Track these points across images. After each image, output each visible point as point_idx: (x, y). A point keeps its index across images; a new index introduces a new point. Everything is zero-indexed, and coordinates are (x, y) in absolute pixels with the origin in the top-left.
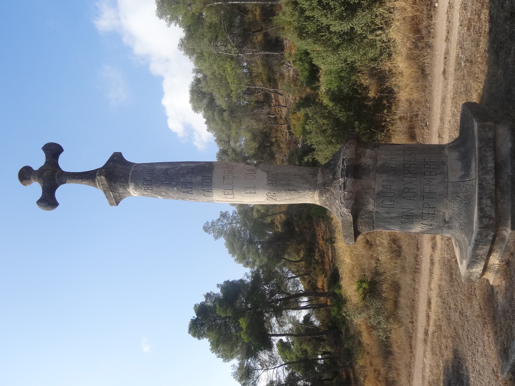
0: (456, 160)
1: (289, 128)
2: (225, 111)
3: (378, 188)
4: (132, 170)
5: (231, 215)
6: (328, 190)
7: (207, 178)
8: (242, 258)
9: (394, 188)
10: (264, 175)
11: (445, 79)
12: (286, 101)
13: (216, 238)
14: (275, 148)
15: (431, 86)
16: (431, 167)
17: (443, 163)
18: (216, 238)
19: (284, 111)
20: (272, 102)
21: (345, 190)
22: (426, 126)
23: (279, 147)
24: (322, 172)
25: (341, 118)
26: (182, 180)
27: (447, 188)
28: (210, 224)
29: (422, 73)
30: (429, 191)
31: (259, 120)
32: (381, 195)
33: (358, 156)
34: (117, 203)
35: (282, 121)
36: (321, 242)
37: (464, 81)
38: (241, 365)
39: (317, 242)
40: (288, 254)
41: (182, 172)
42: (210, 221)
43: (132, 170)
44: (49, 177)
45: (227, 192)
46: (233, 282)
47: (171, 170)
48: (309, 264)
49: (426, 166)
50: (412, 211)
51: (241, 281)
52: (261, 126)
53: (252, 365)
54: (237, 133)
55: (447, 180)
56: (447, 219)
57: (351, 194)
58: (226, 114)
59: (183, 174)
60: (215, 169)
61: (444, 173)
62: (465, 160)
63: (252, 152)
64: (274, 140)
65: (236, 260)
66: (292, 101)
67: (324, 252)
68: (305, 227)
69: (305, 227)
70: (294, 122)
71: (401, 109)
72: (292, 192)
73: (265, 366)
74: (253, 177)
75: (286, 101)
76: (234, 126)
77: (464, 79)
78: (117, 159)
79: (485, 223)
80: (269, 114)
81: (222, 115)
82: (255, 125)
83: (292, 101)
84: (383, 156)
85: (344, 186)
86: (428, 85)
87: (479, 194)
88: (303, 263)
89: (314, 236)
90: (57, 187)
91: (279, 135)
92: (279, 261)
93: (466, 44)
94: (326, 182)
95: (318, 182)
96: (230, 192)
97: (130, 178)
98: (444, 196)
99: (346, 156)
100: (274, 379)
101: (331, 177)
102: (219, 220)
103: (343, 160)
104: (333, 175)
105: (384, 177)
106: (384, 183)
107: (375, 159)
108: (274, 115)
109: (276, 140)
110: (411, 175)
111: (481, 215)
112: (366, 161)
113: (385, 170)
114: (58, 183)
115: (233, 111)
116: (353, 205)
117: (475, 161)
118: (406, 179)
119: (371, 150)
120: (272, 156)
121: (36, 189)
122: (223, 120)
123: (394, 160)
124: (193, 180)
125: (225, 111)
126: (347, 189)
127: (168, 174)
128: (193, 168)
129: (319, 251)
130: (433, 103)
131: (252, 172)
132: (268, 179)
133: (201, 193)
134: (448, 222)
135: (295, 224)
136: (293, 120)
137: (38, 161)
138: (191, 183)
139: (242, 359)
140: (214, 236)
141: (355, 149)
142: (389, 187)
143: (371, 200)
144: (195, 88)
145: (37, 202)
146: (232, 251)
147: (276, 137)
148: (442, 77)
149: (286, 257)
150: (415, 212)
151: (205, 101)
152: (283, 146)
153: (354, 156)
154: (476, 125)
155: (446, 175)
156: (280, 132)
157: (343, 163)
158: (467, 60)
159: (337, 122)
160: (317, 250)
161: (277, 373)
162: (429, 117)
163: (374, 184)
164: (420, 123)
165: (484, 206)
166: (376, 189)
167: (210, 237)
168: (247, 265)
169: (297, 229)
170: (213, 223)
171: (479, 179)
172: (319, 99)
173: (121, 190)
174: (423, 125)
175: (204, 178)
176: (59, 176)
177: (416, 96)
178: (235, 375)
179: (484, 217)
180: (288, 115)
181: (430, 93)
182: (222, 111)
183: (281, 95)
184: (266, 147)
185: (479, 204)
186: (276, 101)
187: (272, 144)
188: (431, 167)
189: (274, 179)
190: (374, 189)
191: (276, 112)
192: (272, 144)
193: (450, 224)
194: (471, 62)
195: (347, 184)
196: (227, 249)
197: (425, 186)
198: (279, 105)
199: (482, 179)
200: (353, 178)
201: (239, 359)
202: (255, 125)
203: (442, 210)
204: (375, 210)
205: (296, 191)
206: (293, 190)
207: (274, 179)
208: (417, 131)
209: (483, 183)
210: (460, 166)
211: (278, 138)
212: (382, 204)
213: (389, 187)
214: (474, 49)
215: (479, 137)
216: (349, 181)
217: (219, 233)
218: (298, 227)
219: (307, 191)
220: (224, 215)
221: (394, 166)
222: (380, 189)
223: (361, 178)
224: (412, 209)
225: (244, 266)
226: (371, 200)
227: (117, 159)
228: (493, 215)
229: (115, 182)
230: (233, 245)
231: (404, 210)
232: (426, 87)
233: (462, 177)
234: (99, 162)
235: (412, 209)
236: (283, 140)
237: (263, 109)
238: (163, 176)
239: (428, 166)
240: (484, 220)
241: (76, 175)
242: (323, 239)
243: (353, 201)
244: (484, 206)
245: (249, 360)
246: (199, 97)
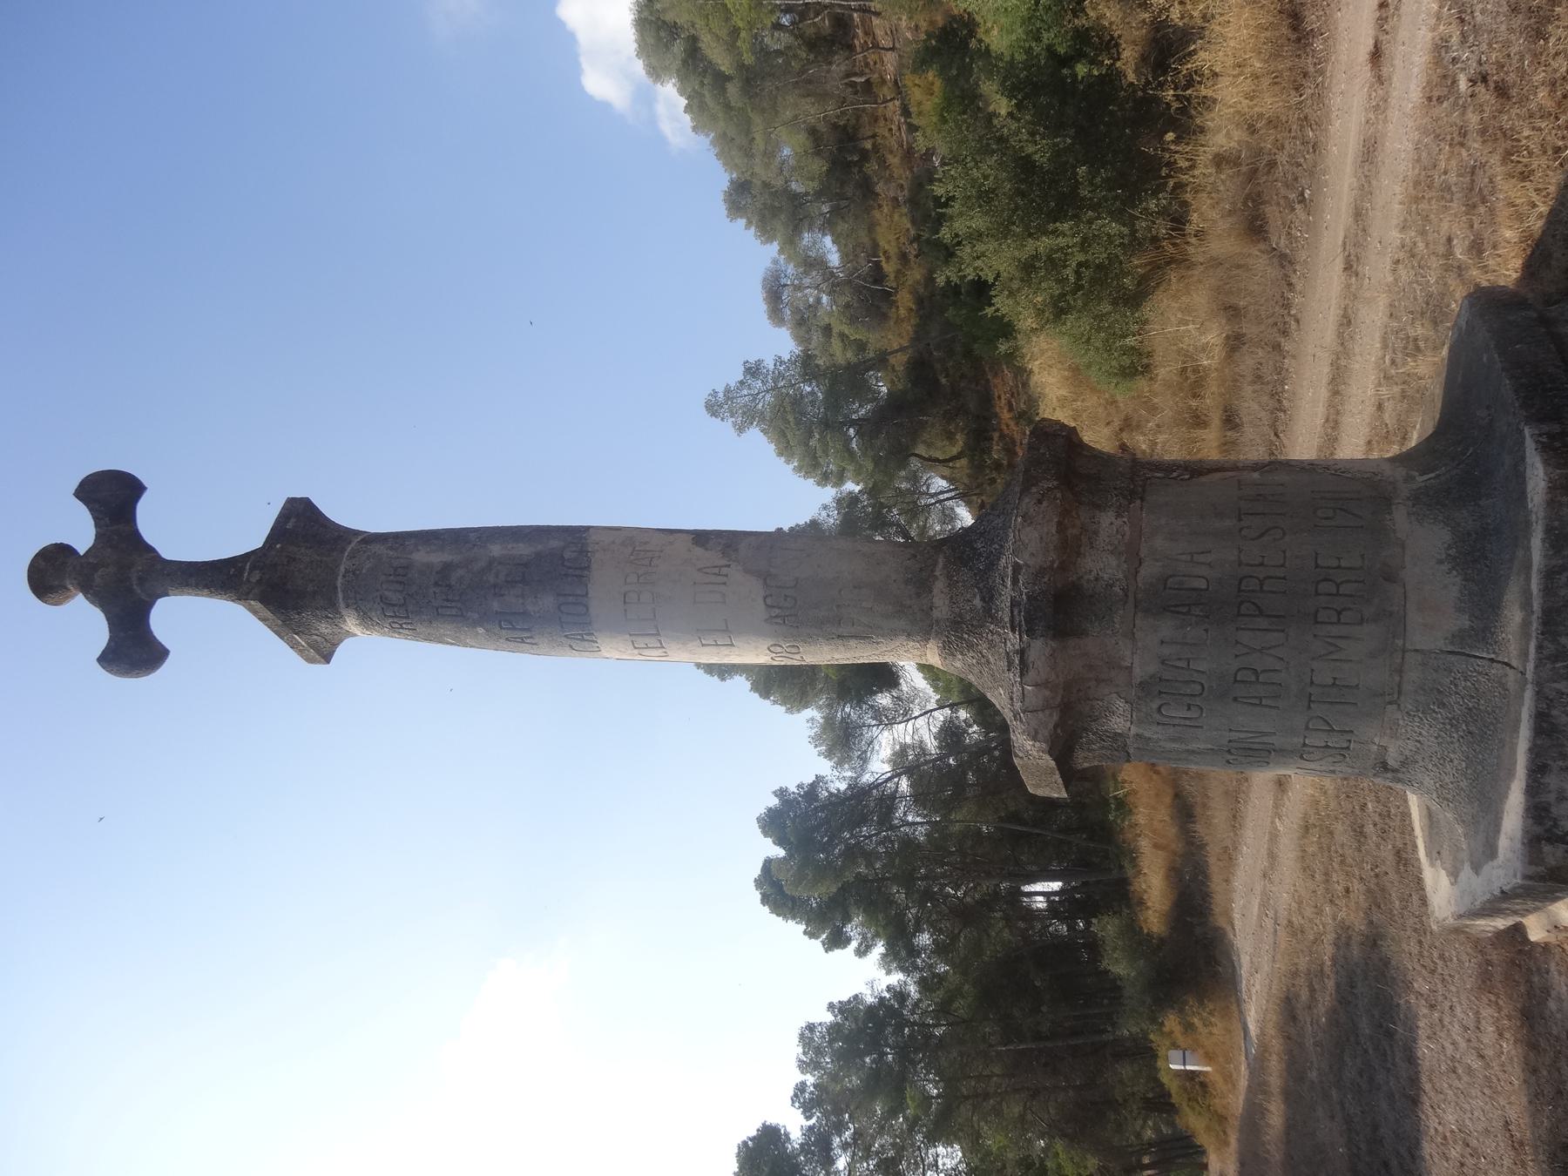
0: (1440, 562)
1: (906, 112)
2: (729, 78)
3: (1143, 667)
4: (342, 569)
5: (771, 367)
6: (971, 646)
7: (571, 599)
8: (812, 466)
9: (1203, 666)
11: (1380, 80)
12: (894, 32)
13: (741, 429)
14: (872, 167)
15: (1322, 72)
17: (1390, 577)
18: (741, 429)
19: (890, 61)
20: (855, 36)
21: (1028, 678)
22: (1302, 200)
23: (883, 162)
24: (949, 577)
25: (1036, 157)
26: (496, 605)
27: (1400, 672)
28: (721, 395)
29: (1295, 28)
30: (1330, 681)
31: (823, 97)
32: (1148, 688)
33: (1069, 547)
34: (327, 658)
35: (885, 90)
36: (1006, 415)
37: (1464, 153)
38: (829, 722)
39: (996, 415)
40: (924, 442)
41: (492, 579)
42: (721, 389)
43: (342, 569)
44: (114, 572)
45: (641, 642)
46: (791, 529)
47: (460, 572)
48: (978, 468)
49: (1323, 587)
50: (1265, 739)
51: (814, 524)
52: (831, 110)
53: (854, 716)
54: (768, 140)
55: (1400, 642)
56: (1391, 763)
57: (1047, 693)
58: (733, 90)
59: (495, 586)
60: (594, 566)
61: (1391, 614)
62: (1480, 562)
63: (813, 185)
64: (868, 145)
65: (798, 469)
66: (909, 35)
67: (1013, 442)
68: (963, 376)
69: (963, 376)
70: (916, 94)
71: (1222, 132)
72: (853, 643)
73: (886, 719)
75: (894, 32)
76: (757, 119)
77: (1462, 145)
78: (301, 524)
79: (1551, 861)
80: (848, 75)
81: (724, 90)
82: (812, 112)
83: (909, 35)
85: (1022, 661)
86: (1311, 69)
87: (1535, 752)
88: (964, 462)
89: (987, 400)
91: (881, 130)
92: (903, 464)
93: (1483, 12)
94: (960, 615)
95: (936, 614)
96: (653, 642)
97: (340, 595)
98: (1388, 698)
99: (1026, 556)
100: (908, 740)
101: (977, 602)
102: (742, 383)
103: (1017, 569)
104: (983, 599)
105: (1167, 627)
107: (1132, 555)
108: (862, 74)
109: (874, 145)
110: (1263, 623)
111: (1539, 830)
112: (1101, 566)
113: (1170, 600)
115: (751, 79)
116: (1055, 727)
117: (1526, 605)
119: (1118, 516)
120: (867, 190)
122: (727, 107)
123: (1202, 558)
124: (530, 608)
125: (729, 78)
126: (1032, 675)
127: (449, 586)
128: (526, 565)
129: (1002, 437)
130: (1326, 130)
131: (713, 579)
132: (769, 601)
133: (561, 645)
135: (938, 366)
136: (916, 89)
138: (525, 614)
139: (830, 706)
140: (734, 424)
141: (1059, 524)
142: (1183, 664)
143: (1120, 704)
144: (646, 14)
145: (99, 660)
146: (785, 450)
147: (874, 136)
148: (1365, 72)
149: (921, 450)
150: (1277, 741)
151: (678, 47)
152: (894, 161)
153: (1053, 556)
154: (1537, 477)
156: (882, 123)
157: (1015, 581)
158: (1484, 79)
159: (1026, 166)
160: (996, 435)
161: (915, 731)
162: (1312, 174)
163: (1128, 653)
164: (1283, 191)
165: (1552, 798)
166: (1137, 671)
167: (726, 427)
168: (824, 479)
169: (944, 381)
170: (728, 390)
171: (1539, 694)
172: (980, 41)
173: (324, 628)
174: (1293, 196)
176: (142, 581)
177: (1269, 104)
178: (816, 740)
179: (1549, 840)
180: (900, 73)
181: (1319, 97)
182: (721, 79)
183: (878, 14)
184: (849, 165)
185: (1532, 790)
186: (866, 33)
187: (865, 156)
190: (1130, 669)
191: (867, 65)
192: (865, 156)
194: (1502, 91)
195: (1032, 655)
196: (773, 446)
198: (876, 46)
199: (1552, 695)
200: (1054, 637)
201: (820, 708)
202: (812, 112)
203: (1376, 740)
204: (1134, 730)
205: (864, 638)
206: (855, 637)
208: (1271, 211)
209: (1555, 712)
211: (879, 140)
212: (1157, 716)
213: (1185, 610)
214: (1519, 44)
215: (1549, 530)
216: (1039, 649)
217: (748, 417)
218: (947, 376)
219: (902, 639)
220: (753, 370)
221: (1202, 584)
222: (1153, 668)
225: (818, 484)
226: (1120, 704)
227: (301, 524)
229: (299, 609)
230: (784, 435)
231: (1234, 736)
232: (1305, 75)
233: (1460, 637)
234: (244, 531)
236: (893, 143)
237: (830, 63)
238: (437, 590)
240: (1547, 848)
242: (1011, 409)
243: (1055, 717)
244: (1552, 798)
245: (847, 710)
246: (659, 39)
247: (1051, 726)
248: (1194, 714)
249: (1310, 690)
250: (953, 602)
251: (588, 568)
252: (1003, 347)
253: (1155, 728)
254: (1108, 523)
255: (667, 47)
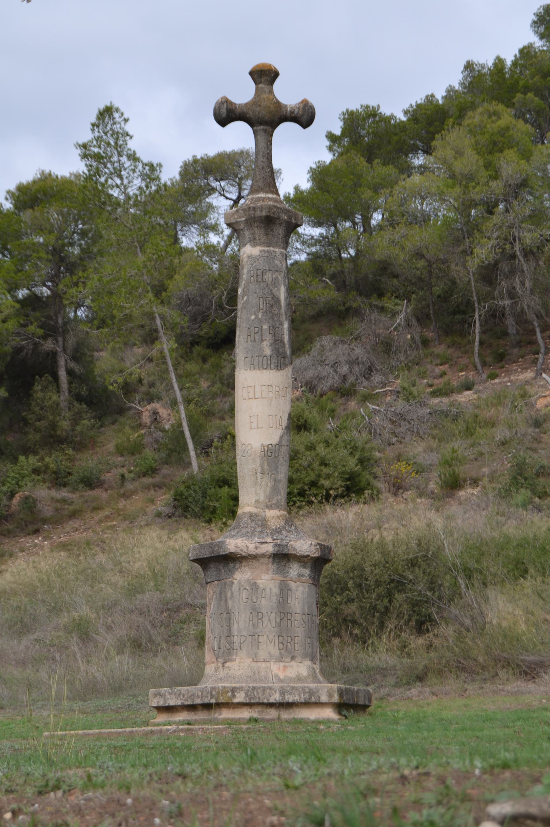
7: (269, 362)
10: (275, 440)
16: (289, 644)
17: (293, 658)
24: (281, 516)
27: (264, 661)
43: (277, 250)
49: (289, 638)
60: (282, 372)
74: (271, 426)
84: (301, 589)
90: (252, 125)
97: (266, 249)
105: (276, 590)
106: (268, 590)
110: (278, 620)
114: (255, 128)
118: (273, 615)
121: (244, 93)
132: (270, 446)
134: (223, 666)
137: (286, 93)
142: (263, 596)
155: (280, 660)
175: (269, 358)
188: (289, 644)
189: (269, 454)
193: (221, 668)
197: (265, 636)
207: (269, 454)
210: (290, 675)
221: (289, 602)
222: (261, 586)
223: (273, 564)
224: (238, 623)
228: (236, 700)
235: (238, 623)
239: (289, 641)
241: (268, 158)
247: (241, 553)
248: (244, 600)
249: (256, 636)
250: (273, 517)
251: (281, 369)
252: (31, 500)
253: (237, 588)
254: (307, 572)
255: (171, 179)
